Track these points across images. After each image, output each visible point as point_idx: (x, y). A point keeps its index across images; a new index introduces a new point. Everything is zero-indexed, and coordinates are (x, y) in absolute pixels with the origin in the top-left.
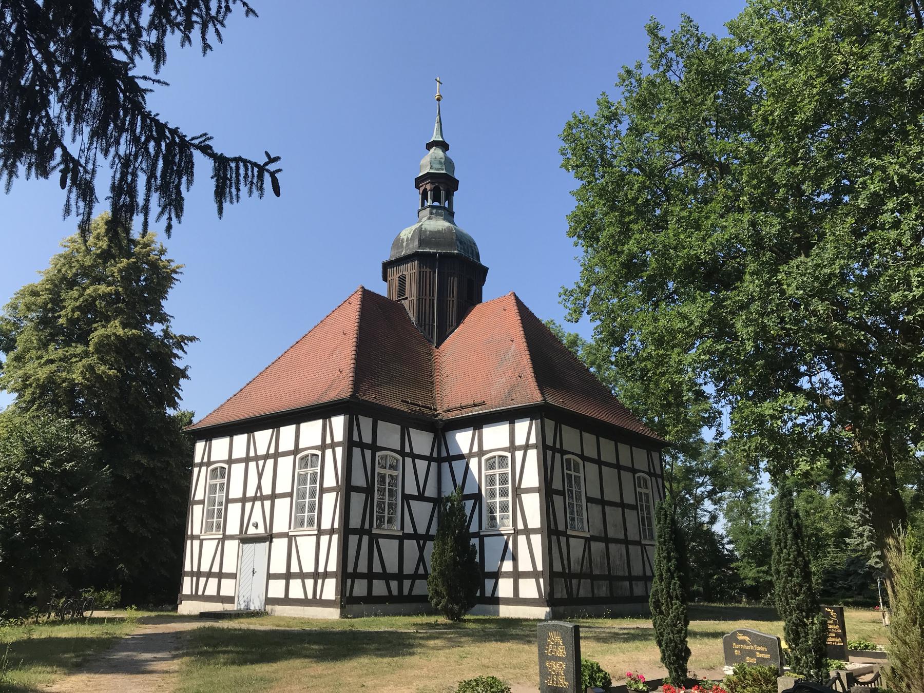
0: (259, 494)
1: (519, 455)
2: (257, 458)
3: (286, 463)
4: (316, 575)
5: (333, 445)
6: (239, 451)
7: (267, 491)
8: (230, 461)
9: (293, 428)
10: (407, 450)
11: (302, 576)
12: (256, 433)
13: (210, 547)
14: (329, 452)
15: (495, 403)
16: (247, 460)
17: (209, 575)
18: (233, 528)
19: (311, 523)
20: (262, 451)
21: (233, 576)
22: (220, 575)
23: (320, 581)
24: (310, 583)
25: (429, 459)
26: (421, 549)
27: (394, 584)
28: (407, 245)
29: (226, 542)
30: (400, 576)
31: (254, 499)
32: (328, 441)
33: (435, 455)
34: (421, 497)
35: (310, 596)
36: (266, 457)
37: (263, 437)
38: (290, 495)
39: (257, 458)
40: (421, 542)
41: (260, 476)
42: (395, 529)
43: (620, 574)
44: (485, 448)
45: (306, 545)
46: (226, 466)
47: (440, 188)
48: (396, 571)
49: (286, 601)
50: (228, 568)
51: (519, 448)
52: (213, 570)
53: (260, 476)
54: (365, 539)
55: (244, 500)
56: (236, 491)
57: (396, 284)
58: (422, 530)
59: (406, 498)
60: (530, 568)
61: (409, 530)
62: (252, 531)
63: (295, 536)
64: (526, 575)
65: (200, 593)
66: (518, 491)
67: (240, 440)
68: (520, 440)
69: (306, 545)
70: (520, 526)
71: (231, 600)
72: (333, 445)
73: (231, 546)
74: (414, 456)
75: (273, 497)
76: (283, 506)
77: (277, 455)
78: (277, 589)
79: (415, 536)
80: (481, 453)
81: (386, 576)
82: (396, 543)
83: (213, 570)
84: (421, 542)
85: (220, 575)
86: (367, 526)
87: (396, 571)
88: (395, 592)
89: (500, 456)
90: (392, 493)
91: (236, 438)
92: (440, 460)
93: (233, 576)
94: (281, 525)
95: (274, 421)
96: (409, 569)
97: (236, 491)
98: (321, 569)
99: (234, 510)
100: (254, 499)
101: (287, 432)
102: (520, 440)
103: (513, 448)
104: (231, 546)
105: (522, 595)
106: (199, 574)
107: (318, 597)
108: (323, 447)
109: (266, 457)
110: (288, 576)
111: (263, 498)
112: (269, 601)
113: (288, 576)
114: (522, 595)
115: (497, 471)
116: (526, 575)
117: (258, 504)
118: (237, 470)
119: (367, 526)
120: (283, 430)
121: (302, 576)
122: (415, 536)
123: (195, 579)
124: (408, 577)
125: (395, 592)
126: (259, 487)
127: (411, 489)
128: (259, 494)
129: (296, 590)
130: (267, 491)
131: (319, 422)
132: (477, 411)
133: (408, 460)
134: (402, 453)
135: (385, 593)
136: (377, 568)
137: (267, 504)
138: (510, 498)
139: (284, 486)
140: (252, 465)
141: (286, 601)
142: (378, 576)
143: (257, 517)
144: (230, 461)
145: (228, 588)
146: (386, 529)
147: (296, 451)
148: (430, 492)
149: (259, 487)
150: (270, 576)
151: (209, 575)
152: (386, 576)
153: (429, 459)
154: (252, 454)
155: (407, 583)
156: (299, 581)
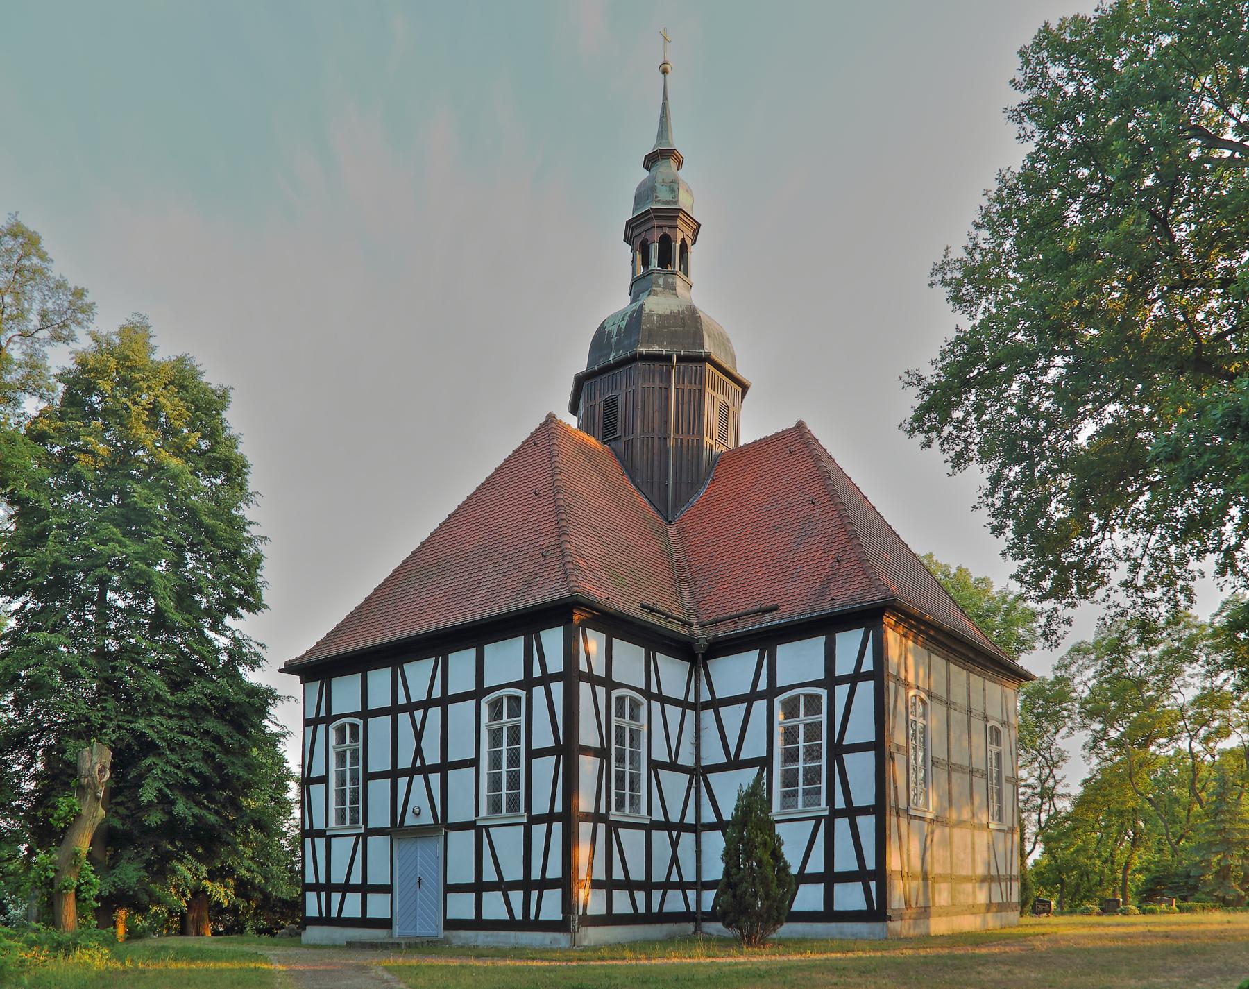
0: (418, 764)
1: (842, 691)
2: (410, 707)
3: (462, 714)
4: (526, 885)
5: (546, 680)
6: (380, 696)
7: (433, 757)
8: (366, 714)
9: (472, 653)
10: (654, 689)
11: (502, 886)
12: (406, 667)
13: (343, 848)
14: (539, 692)
15: (792, 609)
16: (393, 710)
17: (346, 888)
18: (379, 817)
19: (513, 805)
20: (419, 694)
21: (386, 889)
22: (365, 889)
23: (534, 894)
24: (517, 897)
25: (683, 704)
27: (640, 896)
28: (619, 341)
29: (370, 840)
30: (647, 886)
31: (411, 772)
32: (537, 672)
33: (691, 699)
34: (673, 766)
35: (519, 915)
36: (427, 704)
37: (419, 674)
38: (369, 776)
39: (410, 707)
40: (674, 834)
41: (419, 736)
42: (643, 816)
43: (964, 873)
44: (780, 683)
45: (508, 841)
46: (360, 722)
47: (657, 238)
48: (642, 877)
50: (378, 876)
51: (843, 680)
52: (549, 875)
53: (419, 736)
54: (602, 828)
55: (393, 774)
56: (379, 761)
57: (600, 411)
58: (675, 817)
59: (654, 765)
60: (854, 866)
61: (658, 816)
62: (410, 821)
63: (487, 827)
64: (847, 877)
65: (334, 914)
66: (838, 750)
67: (380, 680)
68: (844, 666)
69: (508, 841)
70: (840, 803)
71: (385, 924)
72: (546, 680)
73: (378, 845)
74: (664, 700)
75: (444, 767)
76: (460, 781)
77: (445, 701)
78: (462, 907)
79: (666, 825)
80: (608, 683)
81: (629, 885)
82: (641, 834)
83: (549, 875)
84: (674, 834)
85: (365, 889)
86: (602, 810)
87: (642, 877)
88: (642, 909)
89: (806, 696)
90: (635, 758)
91: (371, 675)
92: (698, 707)
93: (386, 889)
94: (460, 810)
95: (438, 644)
96: (658, 876)
97: (379, 761)
98: (536, 875)
99: (379, 791)
100: (411, 772)
101: (462, 665)
102: (844, 666)
103: (830, 680)
104: (378, 845)
105: (838, 907)
106: (329, 887)
107: (532, 917)
108: (528, 683)
109: (427, 704)
110: (479, 887)
111: (426, 770)
112: (451, 925)
113: (479, 887)
114: (838, 907)
115: (802, 720)
116: (847, 877)
117: (419, 779)
118: (379, 727)
119: (602, 810)
120: (453, 658)
121: (502, 886)
122: (666, 825)
123: (323, 894)
124: (658, 886)
125: (642, 909)
126: (419, 752)
127: (661, 755)
128: (418, 764)
129: (494, 906)
130: (433, 757)
131: (519, 643)
132: (768, 621)
133: (656, 705)
134: (646, 693)
135: (681, 908)
136: (618, 874)
137: (435, 778)
138: (823, 762)
139: (460, 749)
140: (404, 718)
141: (479, 923)
142: (620, 885)
143: (419, 797)
144: (366, 714)
145: (378, 906)
146: (626, 815)
147: (480, 692)
148: (686, 759)
149: (419, 752)
151: (346, 888)
152: (629, 885)
153: (683, 704)
154: (402, 700)
155: (657, 895)
156: (680, 892)
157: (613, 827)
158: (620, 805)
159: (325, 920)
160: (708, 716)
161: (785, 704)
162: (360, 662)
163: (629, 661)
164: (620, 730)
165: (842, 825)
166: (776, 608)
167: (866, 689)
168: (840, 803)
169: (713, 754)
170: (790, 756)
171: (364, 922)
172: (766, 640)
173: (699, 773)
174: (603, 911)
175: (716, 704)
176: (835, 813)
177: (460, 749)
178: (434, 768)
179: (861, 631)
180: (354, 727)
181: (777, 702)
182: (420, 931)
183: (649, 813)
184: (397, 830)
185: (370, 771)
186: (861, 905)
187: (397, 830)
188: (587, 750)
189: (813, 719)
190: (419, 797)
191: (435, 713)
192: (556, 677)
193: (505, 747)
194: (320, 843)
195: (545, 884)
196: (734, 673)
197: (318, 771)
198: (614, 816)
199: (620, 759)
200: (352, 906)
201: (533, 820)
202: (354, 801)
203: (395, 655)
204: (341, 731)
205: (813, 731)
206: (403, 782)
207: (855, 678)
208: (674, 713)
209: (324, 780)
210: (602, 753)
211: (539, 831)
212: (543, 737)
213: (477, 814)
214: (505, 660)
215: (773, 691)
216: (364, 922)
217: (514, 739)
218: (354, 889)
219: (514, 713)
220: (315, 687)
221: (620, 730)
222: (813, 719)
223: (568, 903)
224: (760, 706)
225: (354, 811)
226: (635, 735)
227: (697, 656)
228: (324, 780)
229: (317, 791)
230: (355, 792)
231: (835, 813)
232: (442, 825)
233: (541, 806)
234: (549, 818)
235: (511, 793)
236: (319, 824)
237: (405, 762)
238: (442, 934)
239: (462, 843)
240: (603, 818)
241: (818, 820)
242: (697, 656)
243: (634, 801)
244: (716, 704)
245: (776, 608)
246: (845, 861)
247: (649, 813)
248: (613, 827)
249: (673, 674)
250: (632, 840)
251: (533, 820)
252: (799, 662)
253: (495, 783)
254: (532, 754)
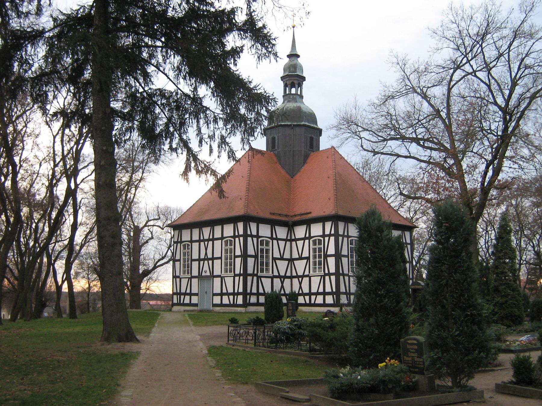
1: (327, 239)
2: (204, 240)
3: (218, 243)
4: (234, 294)
5: (239, 236)
6: (196, 237)
7: (210, 256)
8: (192, 241)
11: (228, 294)
14: (237, 239)
15: (314, 214)
16: (199, 241)
17: (185, 294)
18: (195, 273)
20: (206, 237)
21: (196, 294)
22: (191, 294)
23: (236, 297)
24: (231, 297)
25: (286, 240)
26: (282, 283)
31: (204, 260)
33: (289, 238)
34: (282, 258)
35: (232, 303)
36: (208, 240)
37: (206, 231)
39: (204, 240)
41: (206, 249)
45: (229, 281)
49: (221, 305)
50: (195, 290)
53: (206, 249)
54: (255, 278)
55: (199, 260)
56: (195, 256)
58: (282, 274)
59: (274, 259)
62: (204, 274)
64: (329, 294)
66: (326, 256)
67: (196, 232)
68: (327, 232)
69: (229, 281)
70: (327, 272)
71: (196, 305)
72: (239, 236)
73: (195, 281)
74: (278, 239)
75: (213, 259)
76: (217, 263)
77: (213, 240)
78: (217, 300)
80: (258, 236)
84: (282, 279)
85: (191, 294)
86: (256, 272)
90: (267, 257)
92: (291, 240)
93: (196, 294)
94: (217, 272)
97: (195, 256)
98: (236, 291)
99: (195, 264)
100: (204, 260)
101: (218, 231)
102: (327, 232)
108: (234, 237)
109: (208, 240)
110: (222, 294)
111: (208, 259)
112: (215, 305)
115: (317, 246)
116: (329, 294)
118: (195, 246)
119: (256, 272)
120: (216, 228)
121: (228, 294)
122: (279, 276)
125: (308, 302)
126: (206, 254)
127: (277, 255)
130: (210, 256)
134: (272, 238)
137: (210, 262)
139: (217, 254)
140: (202, 244)
143: (206, 268)
144: (192, 241)
145: (195, 300)
146: (265, 274)
147: (222, 238)
149: (206, 254)
150: (214, 295)
151: (185, 294)
153: (286, 240)
155: (313, 297)
157: (259, 278)
158: (262, 271)
159: (179, 304)
160: (294, 243)
161: (313, 241)
162: (190, 226)
163: (265, 231)
164: (262, 250)
165: (327, 278)
166: (310, 213)
167: (332, 239)
168: (327, 272)
169: (295, 255)
170: (267, 264)
171: (190, 304)
172: (308, 222)
173: (291, 260)
174: (220, 303)
175: (296, 240)
176: (325, 275)
177: (217, 254)
178: (210, 259)
179: (330, 223)
180: (188, 245)
181: (311, 240)
182: (205, 308)
183: (273, 273)
184: (200, 277)
185: (193, 258)
186: (332, 302)
187: (200, 277)
188: (251, 256)
189: (320, 246)
190: (206, 268)
191: (210, 243)
192: (241, 236)
193: (229, 254)
194: (178, 280)
195: (238, 294)
196: (300, 231)
197: (178, 257)
198: (260, 274)
199: (262, 257)
200: (187, 300)
201: (236, 275)
202: (231, 265)
203: (200, 225)
204: (184, 246)
205: (320, 249)
206: (202, 262)
207: (330, 235)
208: (282, 243)
209: (179, 260)
210: (256, 257)
211: (237, 278)
212: (238, 253)
213: (349, 272)
214: (229, 230)
215: (310, 237)
216: (190, 304)
217: (231, 252)
218: (188, 294)
219: (231, 245)
220: (177, 232)
221: (262, 250)
222: (320, 246)
223: (245, 299)
224: (307, 241)
225: (188, 270)
226: (267, 251)
227: (290, 226)
228: (179, 260)
229: (177, 264)
230: (188, 265)
231: (325, 275)
232: (212, 276)
233: (237, 272)
234: (239, 275)
235: (230, 267)
236: (178, 274)
237: (202, 256)
238: (211, 308)
239: (217, 281)
240: (256, 275)
241: (321, 276)
242: (290, 226)
243: (267, 270)
244: (296, 240)
245: (310, 213)
246: (328, 289)
247: (273, 273)
248: (259, 278)
249: (281, 232)
250: (267, 282)
251: (236, 275)
252: (316, 230)
253: (226, 264)
254: (236, 257)
